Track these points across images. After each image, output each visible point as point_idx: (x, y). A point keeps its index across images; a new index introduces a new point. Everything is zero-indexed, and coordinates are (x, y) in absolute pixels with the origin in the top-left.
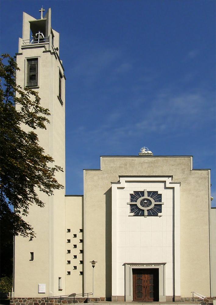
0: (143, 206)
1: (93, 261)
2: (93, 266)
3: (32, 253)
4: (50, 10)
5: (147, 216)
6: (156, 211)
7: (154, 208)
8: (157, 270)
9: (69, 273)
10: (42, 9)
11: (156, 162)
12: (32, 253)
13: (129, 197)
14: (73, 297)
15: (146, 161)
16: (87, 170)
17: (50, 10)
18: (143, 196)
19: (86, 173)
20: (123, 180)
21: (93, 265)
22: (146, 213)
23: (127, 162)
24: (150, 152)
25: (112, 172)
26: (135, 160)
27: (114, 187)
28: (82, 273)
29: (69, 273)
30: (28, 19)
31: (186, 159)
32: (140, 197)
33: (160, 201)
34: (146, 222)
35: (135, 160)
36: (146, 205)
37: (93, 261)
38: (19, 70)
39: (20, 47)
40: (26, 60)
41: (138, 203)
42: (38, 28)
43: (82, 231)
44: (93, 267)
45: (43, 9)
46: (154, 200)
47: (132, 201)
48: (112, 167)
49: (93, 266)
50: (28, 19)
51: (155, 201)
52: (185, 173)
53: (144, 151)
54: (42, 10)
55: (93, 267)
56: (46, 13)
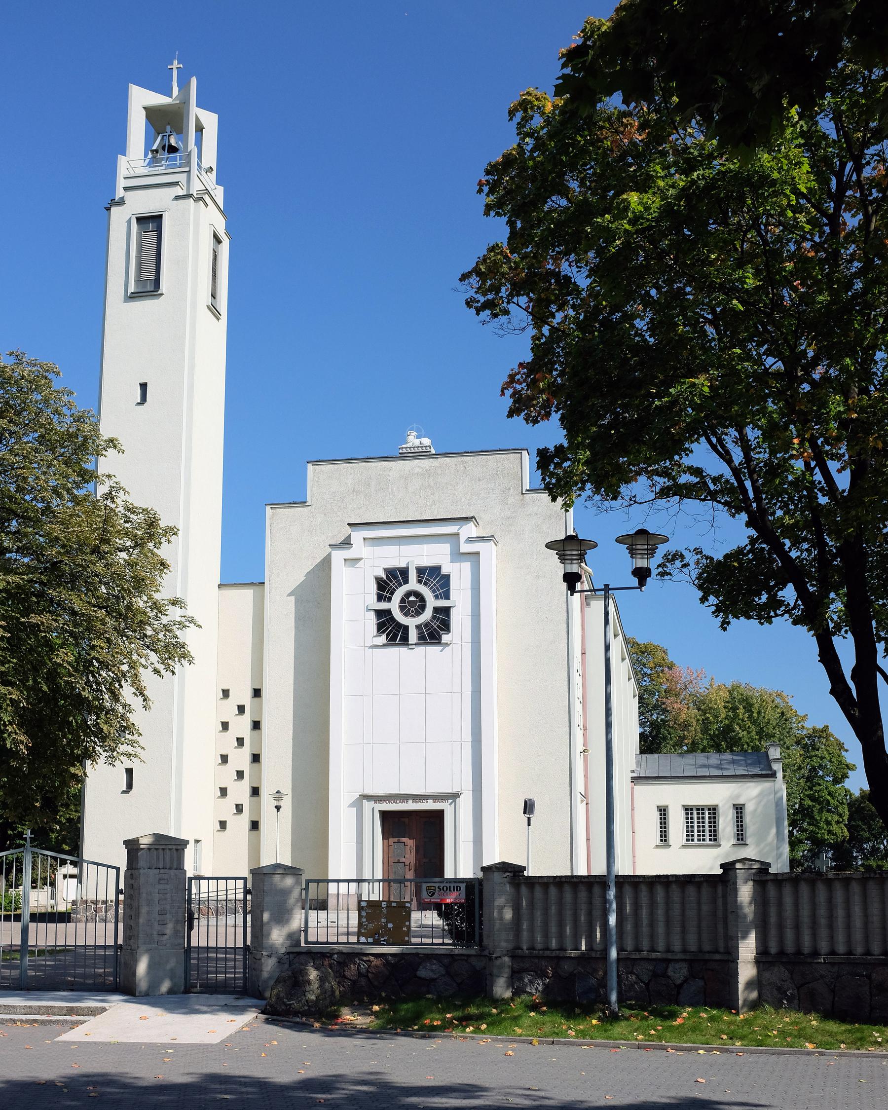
0: (406, 615)
1: (278, 792)
2: (276, 807)
3: (144, 386)
4: (194, 82)
5: (416, 644)
6: (435, 632)
7: (434, 617)
8: (440, 814)
9: (223, 825)
10: (175, 62)
11: (439, 471)
12: (144, 386)
13: (373, 588)
14: (215, 955)
15: (417, 470)
16: (275, 505)
17: (194, 82)
18: (406, 581)
19: (272, 516)
20: (357, 536)
21: (278, 804)
22: (413, 636)
23: (370, 478)
24: (426, 441)
25: (335, 509)
26: (390, 469)
27: (338, 556)
28: (255, 825)
29: (223, 825)
30: (141, 99)
31: (513, 457)
32: (400, 585)
33: (447, 597)
34: (415, 658)
35: (390, 469)
36: (413, 612)
37: (278, 792)
38: (123, 792)
39: (121, 183)
40: (134, 221)
41: (394, 605)
42: (165, 123)
43: (257, 693)
44: (278, 810)
45: (178, 63)
46: (434, 592)
47: (380, 598)
48: (334, 493)
49: (278, 808)
50: (141, 99)
51: (436, 597)
52: (509, 501)
53: (413, 440)
54: (175, 64)
55: (278, 810)
56: (184, 85)
